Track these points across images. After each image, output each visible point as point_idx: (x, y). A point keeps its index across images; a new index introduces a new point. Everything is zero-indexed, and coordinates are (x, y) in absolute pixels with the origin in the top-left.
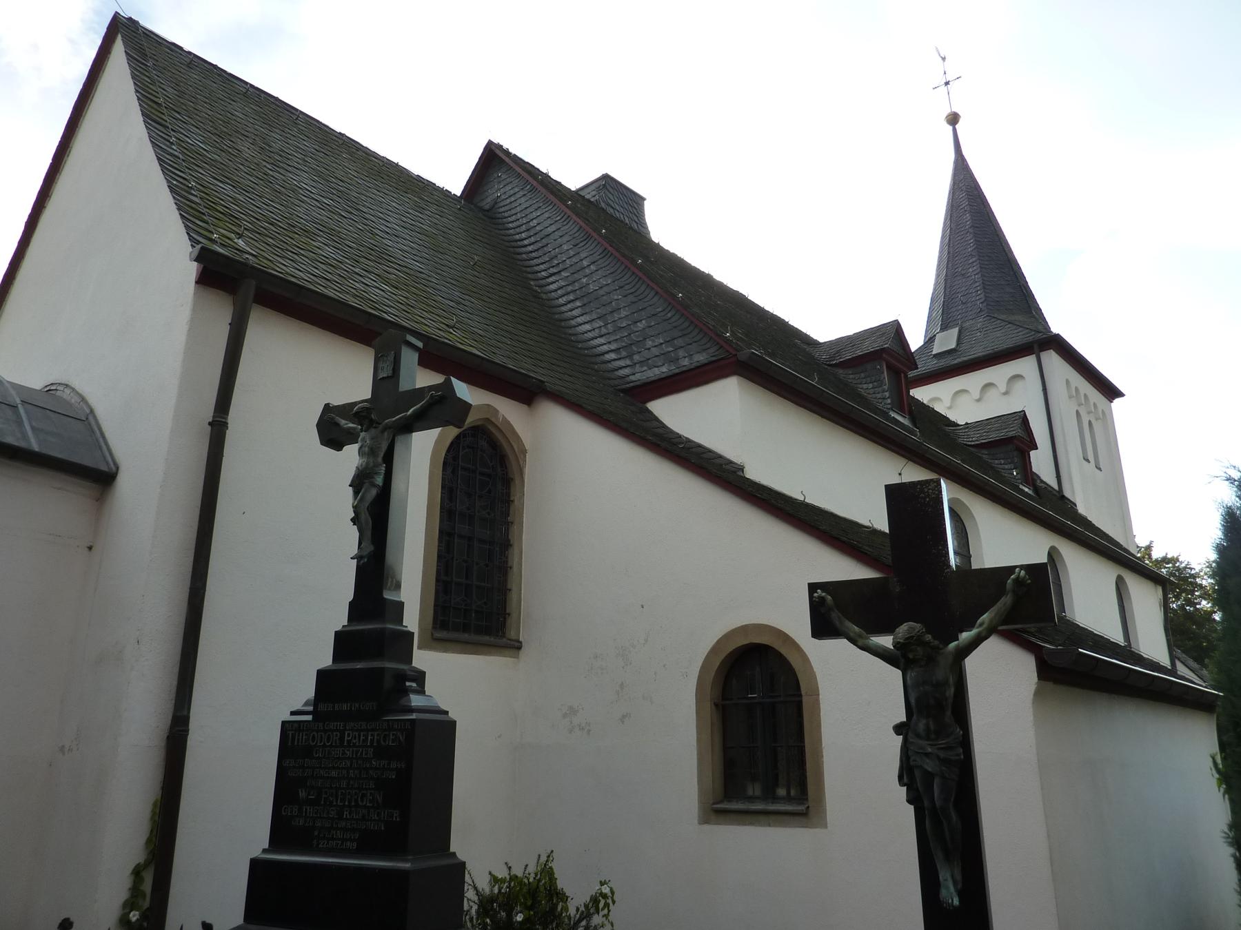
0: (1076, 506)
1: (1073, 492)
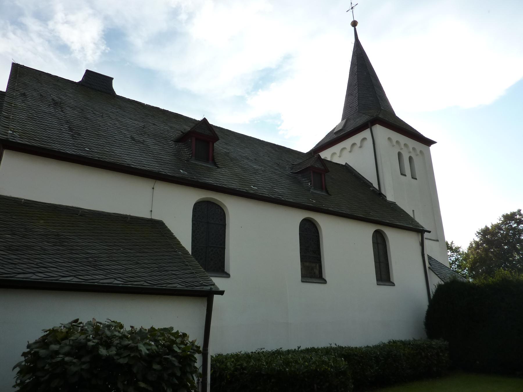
0: (386, 197)
1: (385, 191)
